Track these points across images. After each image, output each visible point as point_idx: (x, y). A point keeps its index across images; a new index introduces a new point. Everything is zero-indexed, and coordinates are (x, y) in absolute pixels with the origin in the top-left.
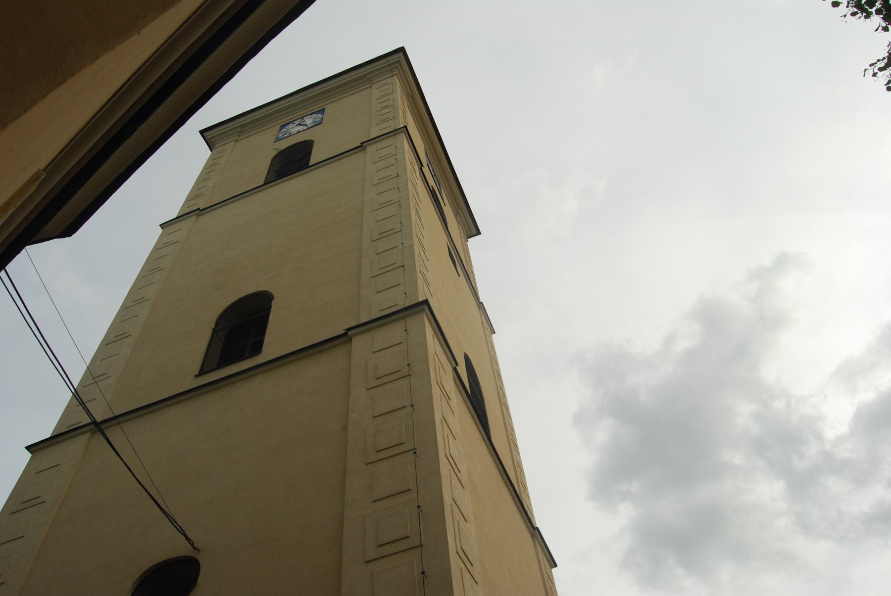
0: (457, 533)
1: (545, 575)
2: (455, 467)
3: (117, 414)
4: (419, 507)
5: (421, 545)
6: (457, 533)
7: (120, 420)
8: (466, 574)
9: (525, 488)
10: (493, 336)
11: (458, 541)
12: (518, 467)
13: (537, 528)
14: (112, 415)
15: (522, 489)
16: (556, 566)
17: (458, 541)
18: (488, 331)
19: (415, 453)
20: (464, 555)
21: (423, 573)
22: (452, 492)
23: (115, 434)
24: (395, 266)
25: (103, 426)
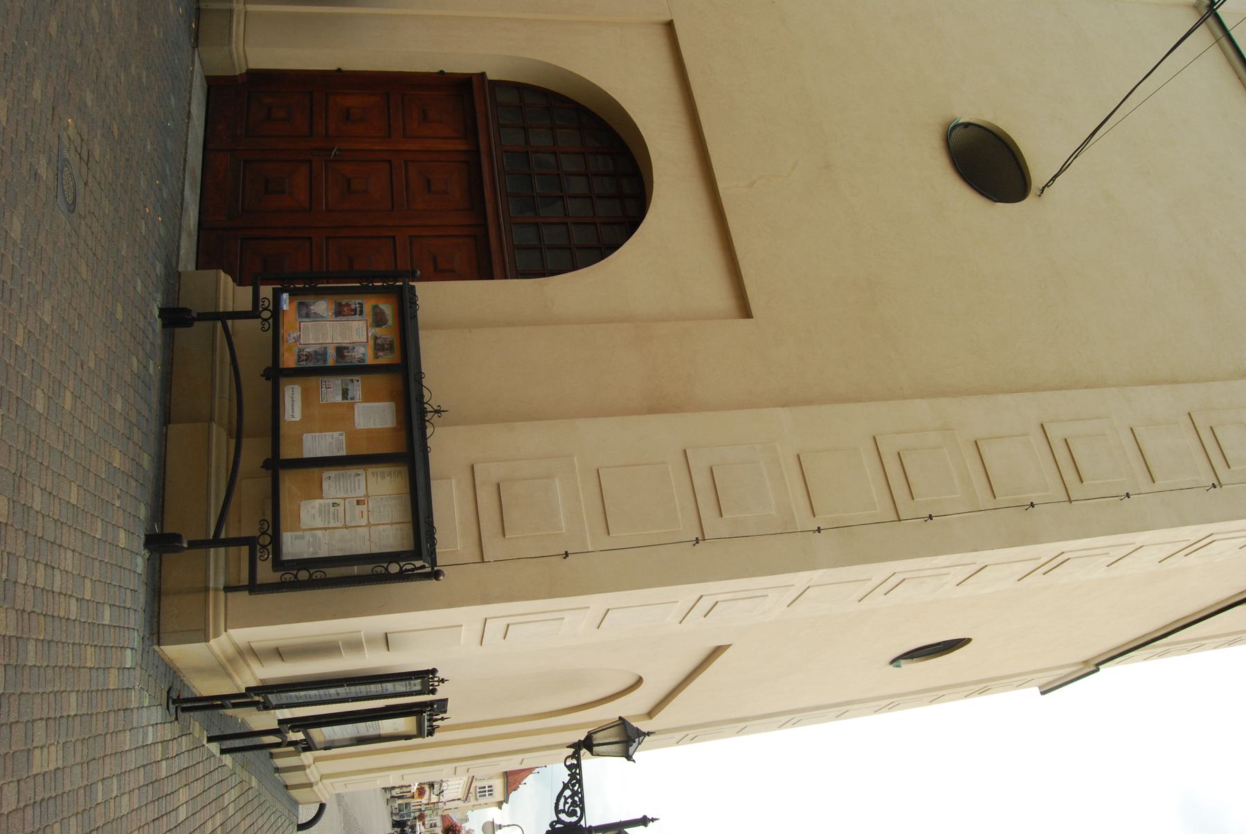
0: (1084, 553)
1: (1029, 677)
2: (1193, 548)
3: (1232, 33)
4: (931, 517)
5: (1070, 501)
6: (935, 572)
7: (1224, 41)
8: (1031, 565)
9: (1160, 655)
10: (1036, 691)
11: (1079, 554)
12: (1198, 645)
13: (1098, 670)
14: (1229, 27)
15: (1158, 650)
16: (1043, 693)
17: (1079, 554)
18: (1046, 678)
19: (697, 541)
20: (1059, 561)
21: (1032, 505)
22: (1155, 543)
23: (1202, 37)
24: (708, 510)
25: (1211, 20)
